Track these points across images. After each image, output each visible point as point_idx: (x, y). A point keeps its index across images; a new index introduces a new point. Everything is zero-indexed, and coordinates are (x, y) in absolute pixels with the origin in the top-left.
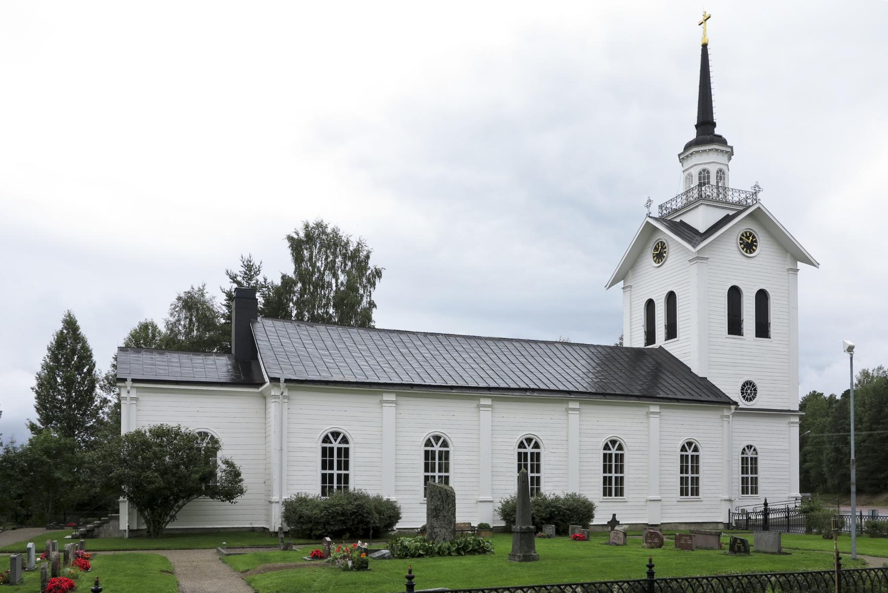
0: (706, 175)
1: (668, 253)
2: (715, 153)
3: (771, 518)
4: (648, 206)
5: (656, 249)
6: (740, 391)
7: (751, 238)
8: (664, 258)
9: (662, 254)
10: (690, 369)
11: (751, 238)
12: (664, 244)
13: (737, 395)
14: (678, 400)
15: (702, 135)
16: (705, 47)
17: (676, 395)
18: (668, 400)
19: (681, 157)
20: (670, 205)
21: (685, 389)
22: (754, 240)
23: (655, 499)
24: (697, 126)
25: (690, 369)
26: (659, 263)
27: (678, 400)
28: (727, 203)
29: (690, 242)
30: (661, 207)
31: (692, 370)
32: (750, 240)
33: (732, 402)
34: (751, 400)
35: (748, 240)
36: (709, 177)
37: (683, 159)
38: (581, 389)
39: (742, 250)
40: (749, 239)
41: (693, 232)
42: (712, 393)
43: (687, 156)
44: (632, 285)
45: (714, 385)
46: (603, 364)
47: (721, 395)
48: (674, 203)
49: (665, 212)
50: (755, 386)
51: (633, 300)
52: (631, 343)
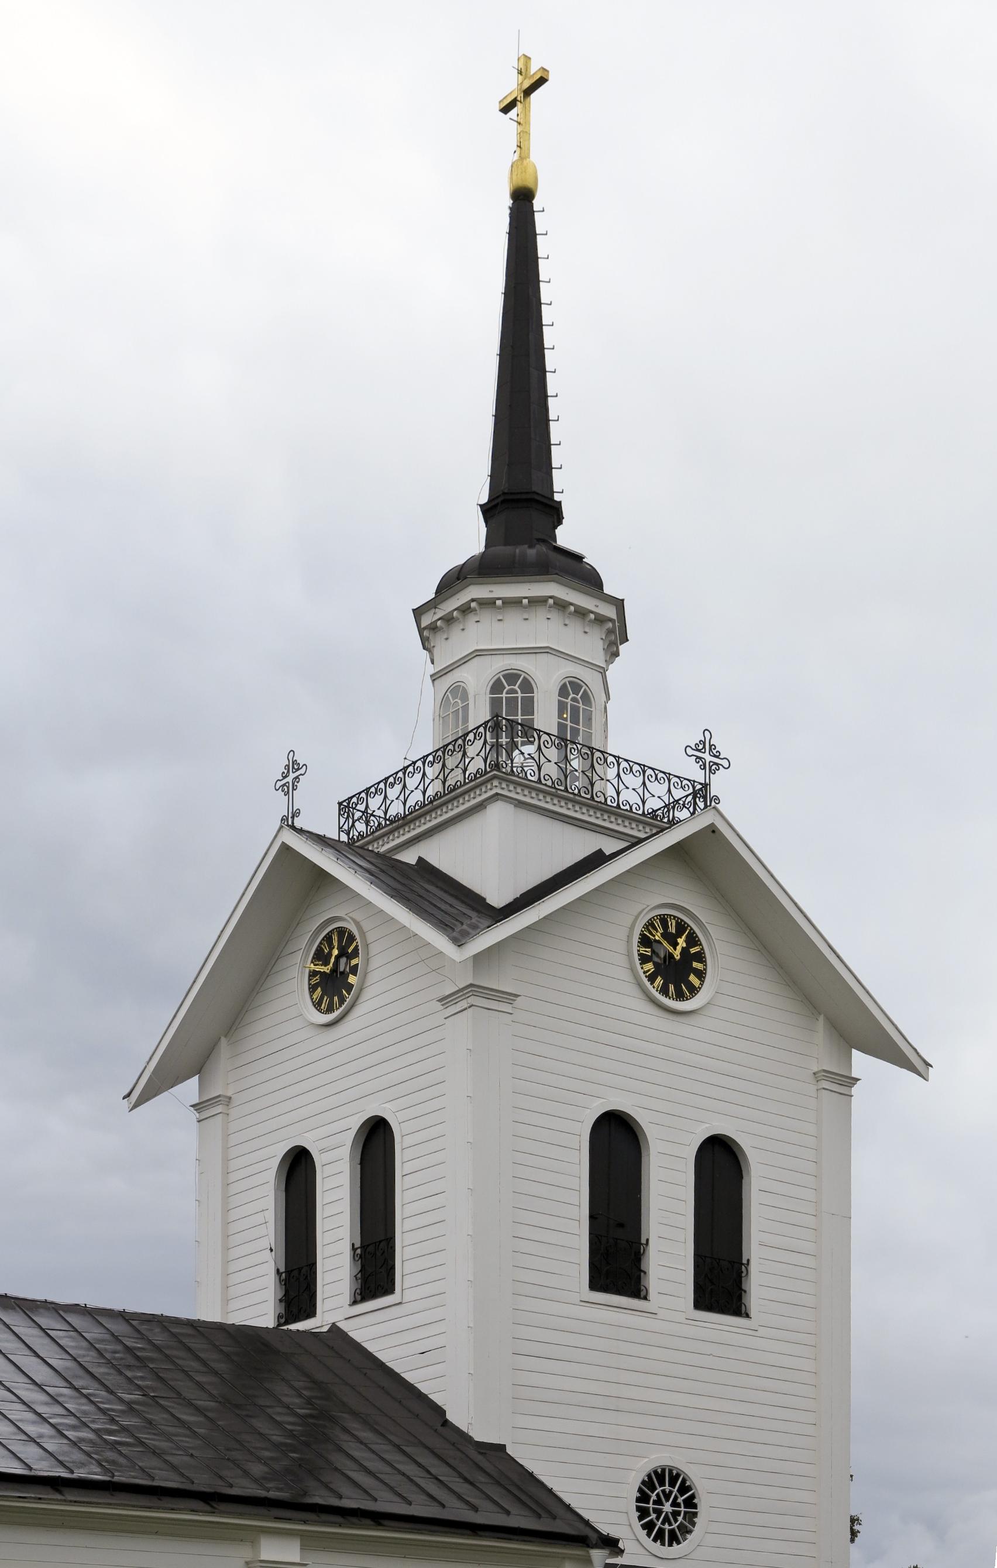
0: (520, 695)
1: (365, 974)
2: (555, 615)
4: (288, 788)
5: (320, 956)
6: (633, 1505)
7: (682, 942)
8: (349, 991)
9: (344, 975)
10: (440, 1412)
11: (682, 942)
12: (352, 938)
13: (622, 1518)
14: (378, 1519)
15: (506, 544)
17: (410, 1503)
18: (339, 1519)
19: (426, 621)
20: (379, 799)
21: (411, 1480)
22: (693, 950)
24: (488, 511)
25: (444, 1412)
26: (330, 1009)
27: (378, 1519)
28: (603, 808)
29: (443, 925)
30: (345, 807)
31: (449, 1417)
32: (679, 948)
33: (593, 1537)
34: (674, 1539)
35: (670, 949)
36: (529, 706)
37: (433, 628)
38: (44, 1468)
39: (648, 984)
40: (675, 945)
41: (463, 902)
42: (519, 1500)
43: (449, 620)
44: (229, 1094)
45: (531, 1475)
46: (81, 1372)
47: (560, 1511)
48: (393, 793)
49: (361, 827)
51: (233, 1152)
52: (226, 1301)
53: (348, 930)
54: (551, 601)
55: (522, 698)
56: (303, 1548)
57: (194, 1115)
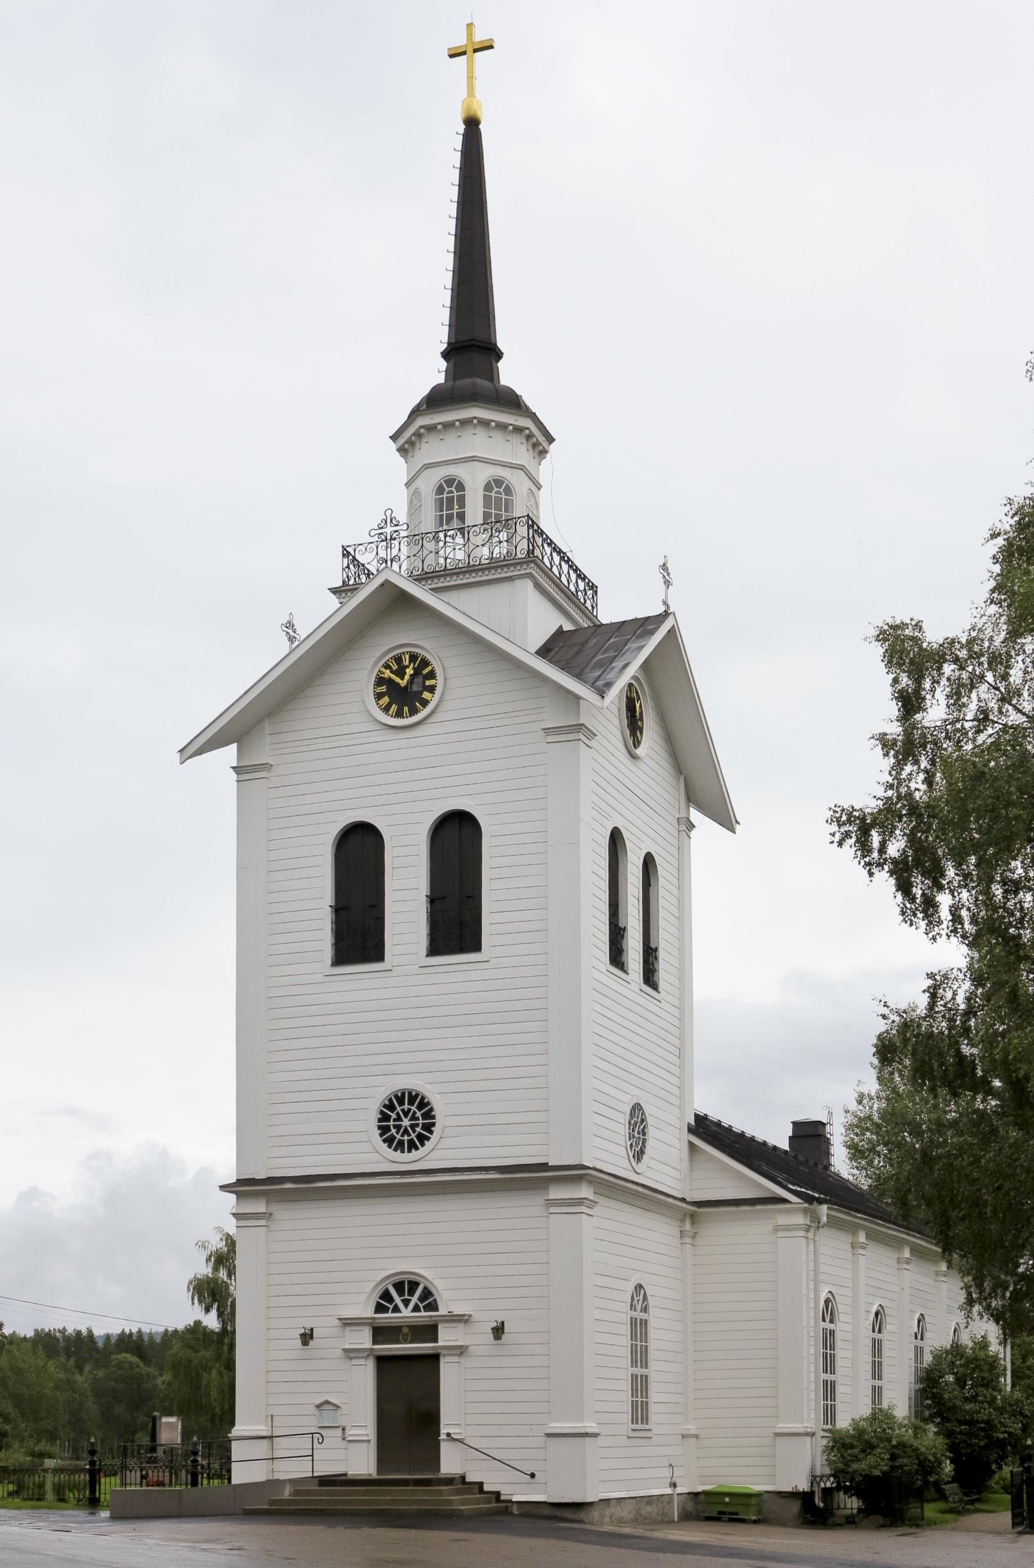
0: (455, 494)
3: (115, 1475)
16: (472, 125)
19: (401, 441)
23: (575, 1431)
24: (446, 355)
36: (462, 501)
50: (417, 1095)
53: (387, 674)
54: (475, 421)
55: (457, 496)
57: (234, 776)
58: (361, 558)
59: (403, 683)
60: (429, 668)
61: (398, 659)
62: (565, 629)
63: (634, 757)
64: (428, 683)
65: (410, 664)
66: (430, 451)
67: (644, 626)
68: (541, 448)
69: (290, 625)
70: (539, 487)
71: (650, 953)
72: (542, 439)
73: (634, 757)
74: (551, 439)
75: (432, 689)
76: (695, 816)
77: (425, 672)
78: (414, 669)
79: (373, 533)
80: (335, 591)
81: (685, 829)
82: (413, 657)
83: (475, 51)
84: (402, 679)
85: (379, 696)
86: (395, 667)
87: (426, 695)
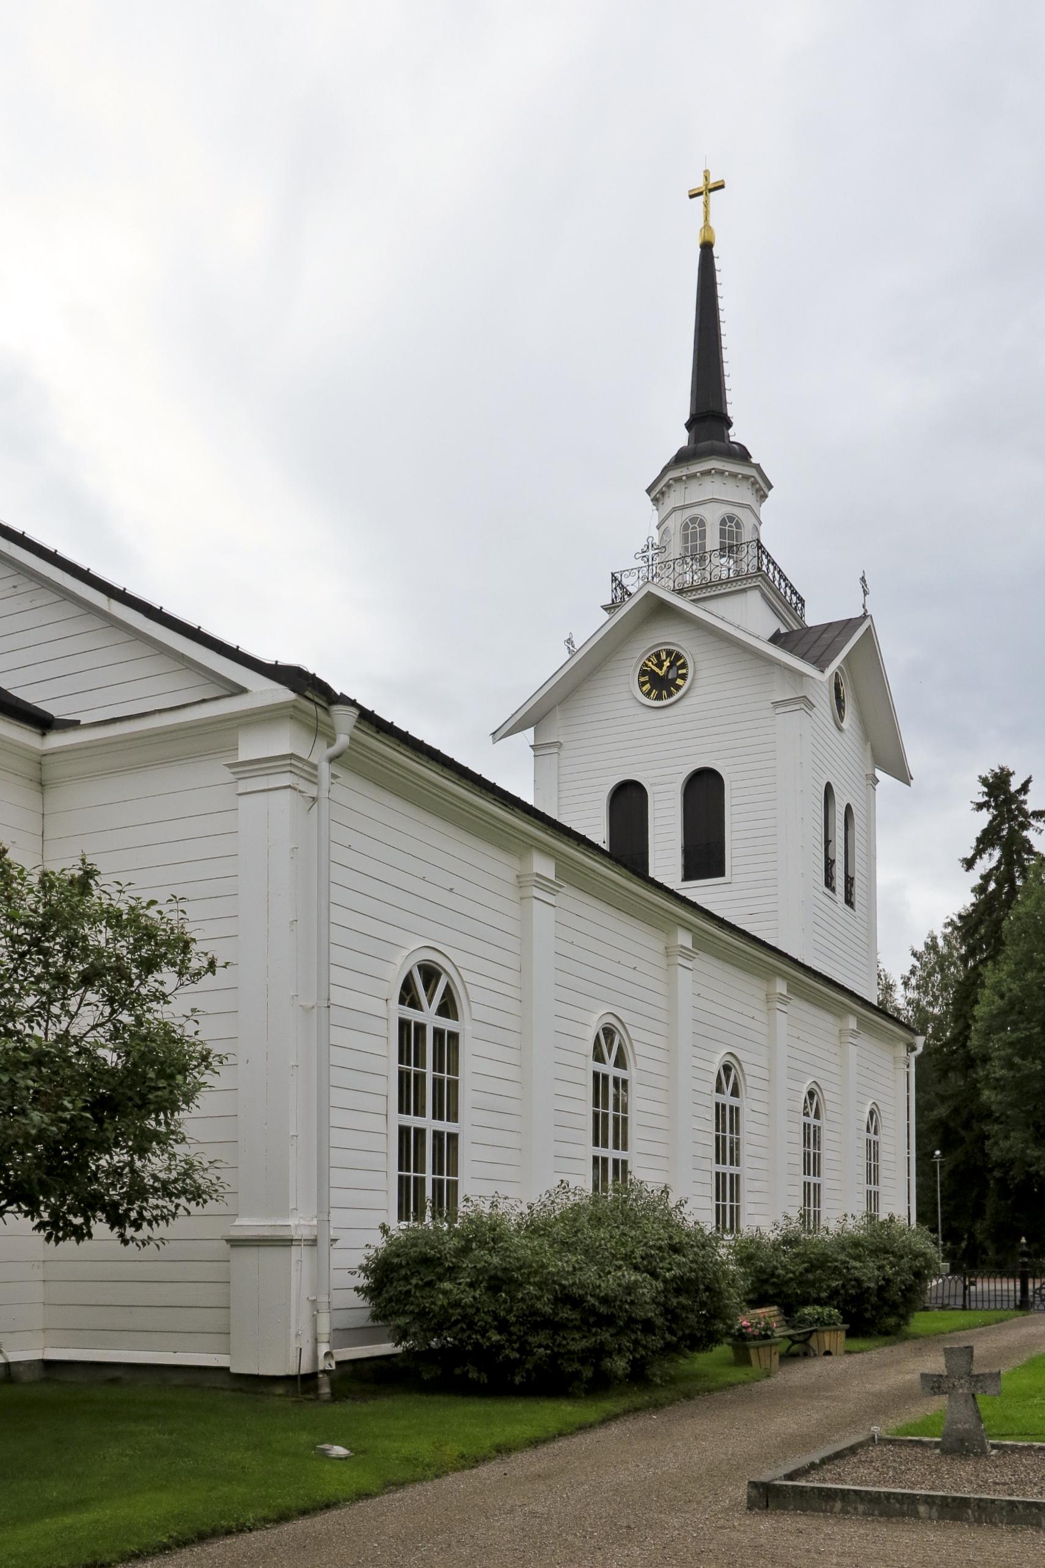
0: (698, 529)
2: (718, 480)
16: (707, 248)
19: (653, 494)
24: (689, 426)
54: (713, 471)
56: (437, 1183)
58: (625, 582)
59: (661, 673)
60: (682, 661)
61: (658, 655)
62: (782, 632)
63: (840, 729)
64: (680, 672)
65: (667, 658)
66: (674, 498)
67: (848, 626)
68: (762, 493)
69: (569, 641)
70: (760, 523)
71: (849, 881)
72: (763, 485)
73: (840, 729)
74: (770, 487)
75: (684, 677)
76: (879, 774)
77: (679, 663)
78: (670, 662)
79: (637, 556)
80: (606, 608)
81: (871, 782)
82: (669, 653)
83: (711, 190)
84: (661, 670)
85: (642, 684)
86: (655, 662)
87: (679, 682)
